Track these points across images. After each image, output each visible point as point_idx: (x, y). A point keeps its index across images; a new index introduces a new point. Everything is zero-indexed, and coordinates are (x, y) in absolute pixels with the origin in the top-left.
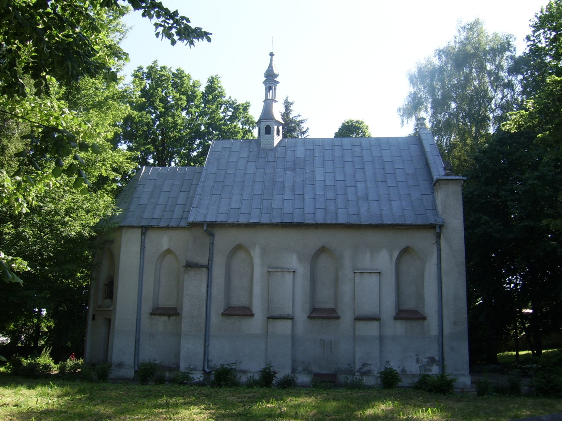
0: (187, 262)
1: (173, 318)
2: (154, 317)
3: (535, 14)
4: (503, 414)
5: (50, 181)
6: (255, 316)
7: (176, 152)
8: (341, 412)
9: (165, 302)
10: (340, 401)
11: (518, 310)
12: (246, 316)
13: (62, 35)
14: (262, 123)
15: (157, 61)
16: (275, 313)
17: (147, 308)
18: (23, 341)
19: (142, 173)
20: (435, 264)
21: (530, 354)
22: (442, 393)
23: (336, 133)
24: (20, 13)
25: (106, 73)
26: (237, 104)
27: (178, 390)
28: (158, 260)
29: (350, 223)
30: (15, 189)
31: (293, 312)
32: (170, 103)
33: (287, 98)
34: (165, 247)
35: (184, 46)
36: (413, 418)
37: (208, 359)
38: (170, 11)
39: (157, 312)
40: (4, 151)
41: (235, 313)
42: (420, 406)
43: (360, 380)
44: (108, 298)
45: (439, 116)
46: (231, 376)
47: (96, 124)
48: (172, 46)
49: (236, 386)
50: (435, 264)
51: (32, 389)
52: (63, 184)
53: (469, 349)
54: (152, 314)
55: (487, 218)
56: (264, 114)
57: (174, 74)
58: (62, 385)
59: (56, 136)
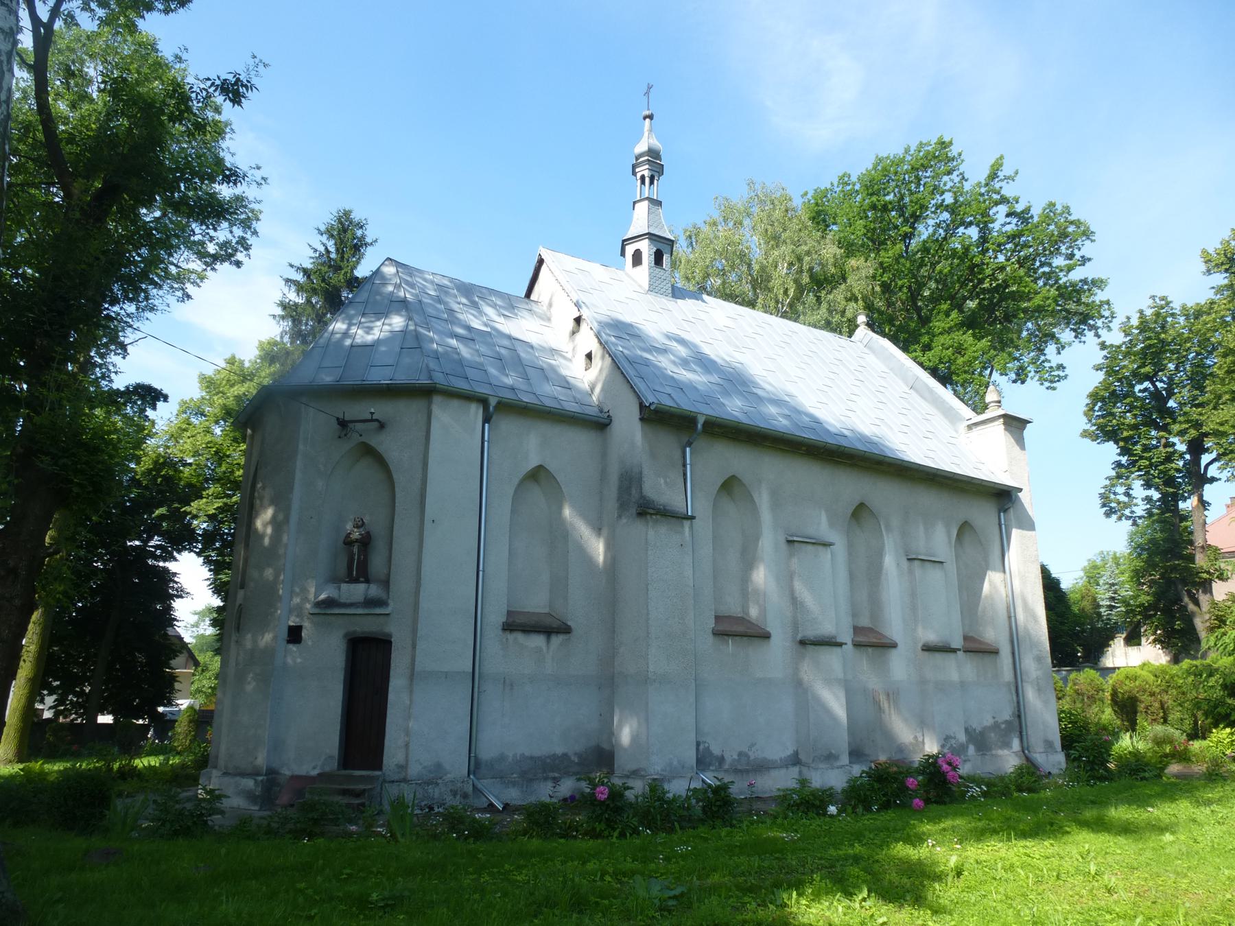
0: (509, 613)
1: (557, 640)
2: (511, 637)
3: (1067, 371)
5: (942, 193)
6: (773, 638)
9: (536, 603)
10: (174, 79)
12: (572, 417)
13: (1099, 410)
14: (627, 247)
16: (811, 633)
17: (495, 616)
18: (92, 408)
20: (244, 192)
21: (130, 541)
22: (1066, 335)
27: (835, 228)
28: (1126, 829)
30: (114, 301)
33: (292, 266)
34: (534, 462)
35: (1034, 421)
39: (515, 625)
40: (88, 77)
41: (874, 640)
44: (362, 579)
47: (1206, 714)
50: (244, 192)
51: (1111, 642)
53: (1045, 602)
54: (509, 627)
55: (361, 336)
56: (961, 481)
57: (1093, 608)
58: (553, 369)
59: (919, 304)
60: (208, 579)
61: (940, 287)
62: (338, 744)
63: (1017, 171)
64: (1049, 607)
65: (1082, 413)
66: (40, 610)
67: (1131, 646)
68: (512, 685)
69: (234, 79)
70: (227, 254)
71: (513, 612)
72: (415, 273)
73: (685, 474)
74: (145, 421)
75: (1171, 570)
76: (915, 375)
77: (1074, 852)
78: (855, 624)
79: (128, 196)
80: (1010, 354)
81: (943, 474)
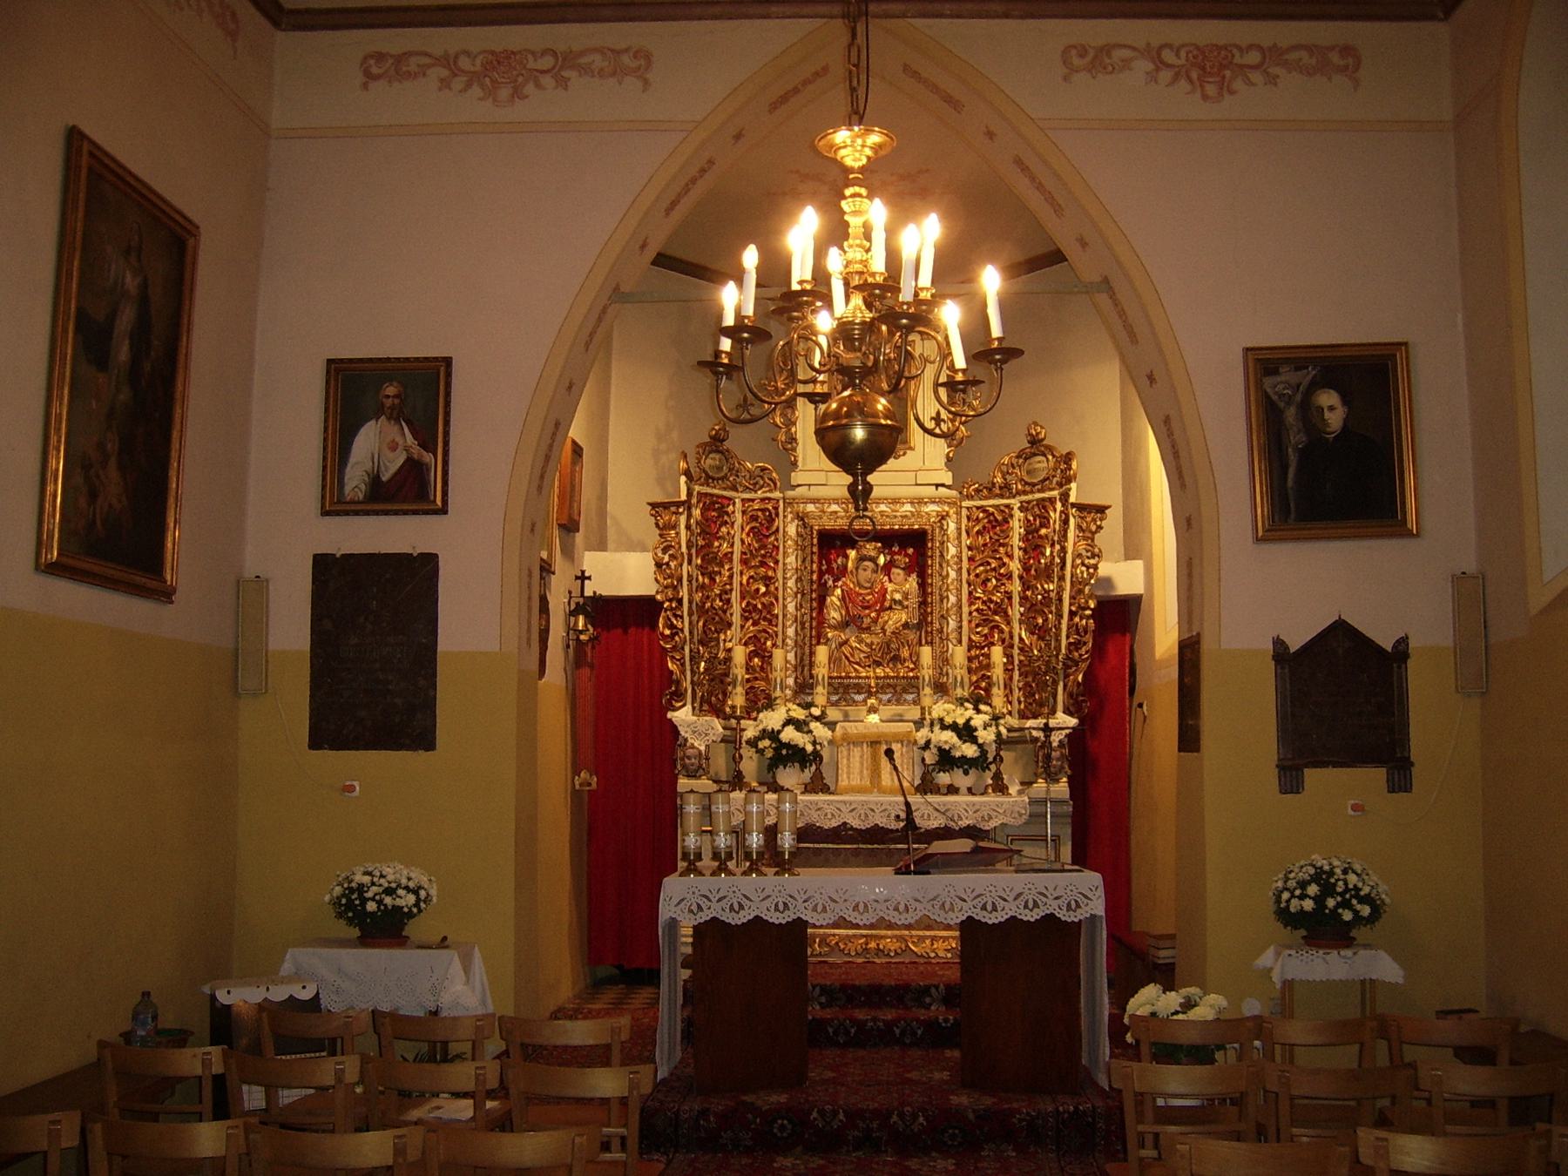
48: (1402, 796)
60: (804, 403)
61: (674, 605)
62: (621, 594)
63: (683, 452)
64: (609, 377)
65: (1416, 765)
66: (875, 138)
67: (1319, 946)
68: (643, 246)
69: (855, 222)
70: (1205, 97)
71: (211, 1039)
72: (1296, 438)
73: (1338, 1099)
74: (839, 452)
75: (803, 85)
76: (1245, 1141)
77: (405, 872)
78: (1123, 558)
79: (778, 474)
80: (680, 746)
81: (187, 276)
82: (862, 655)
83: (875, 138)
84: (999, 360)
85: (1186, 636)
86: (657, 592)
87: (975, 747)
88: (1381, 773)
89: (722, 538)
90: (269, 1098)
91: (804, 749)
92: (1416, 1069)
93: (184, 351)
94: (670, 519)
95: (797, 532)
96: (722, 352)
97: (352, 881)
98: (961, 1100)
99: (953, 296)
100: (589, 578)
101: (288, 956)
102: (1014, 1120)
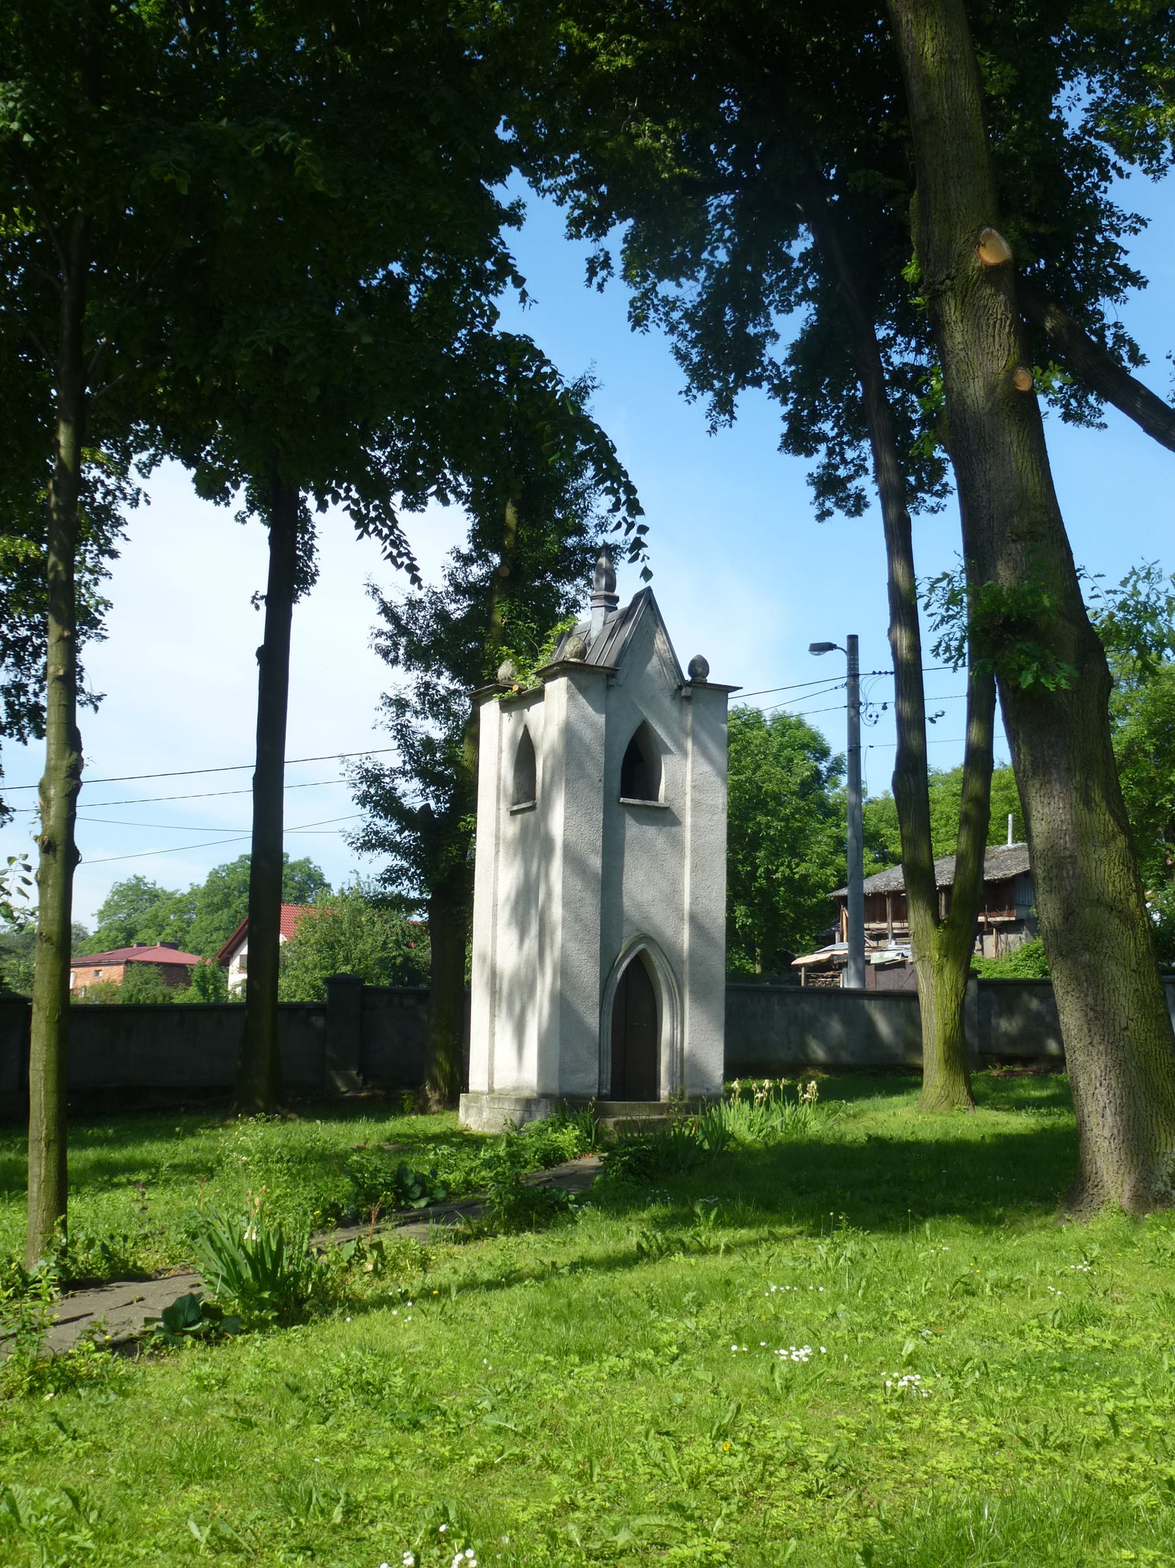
4: (191, 1271)
7: (618, 500)
8: (67, 1261)
11: (758, 167)
15: (1143, 222)
19: (997, 697)
23: (807, 456)
24: (299, 47)
25: (569, 1313)
26: (393, 759)
29: (849, 1138)
31: (501, 718)
32: (1154, 778)
36: (1113, 719)
37: (611, 636)
38: (263, 521)
42: (1083, 1184)
43: (179, 934)
45: (896, 360)
46: (785, 842)
48: (808, 648)
49: (473, 585)
52: (874, 1314)
59: (15, 209)
82: (269, 1450)
83: (802, 228)
84: (802, 410)
85: (74, 931)
86: (404, 762)
87: (907, 1341)
88: (711, 679)
89: (434, 1173)
90: (597, 133)
91: (675, 279)
92: (971, 1094)
93: (118, 1155)
94: (823, 1039)
95: (731, 921)
96: (780, 390)
97: (581, 1398)
98: (990, 582)
99: (1015, 246)
100: (96, 708)
101: (88, 306)
102: (1064, 685)
